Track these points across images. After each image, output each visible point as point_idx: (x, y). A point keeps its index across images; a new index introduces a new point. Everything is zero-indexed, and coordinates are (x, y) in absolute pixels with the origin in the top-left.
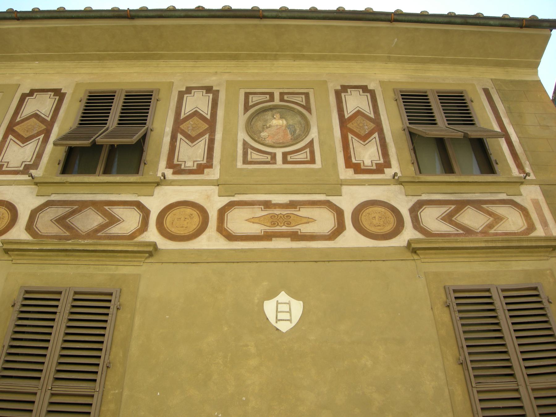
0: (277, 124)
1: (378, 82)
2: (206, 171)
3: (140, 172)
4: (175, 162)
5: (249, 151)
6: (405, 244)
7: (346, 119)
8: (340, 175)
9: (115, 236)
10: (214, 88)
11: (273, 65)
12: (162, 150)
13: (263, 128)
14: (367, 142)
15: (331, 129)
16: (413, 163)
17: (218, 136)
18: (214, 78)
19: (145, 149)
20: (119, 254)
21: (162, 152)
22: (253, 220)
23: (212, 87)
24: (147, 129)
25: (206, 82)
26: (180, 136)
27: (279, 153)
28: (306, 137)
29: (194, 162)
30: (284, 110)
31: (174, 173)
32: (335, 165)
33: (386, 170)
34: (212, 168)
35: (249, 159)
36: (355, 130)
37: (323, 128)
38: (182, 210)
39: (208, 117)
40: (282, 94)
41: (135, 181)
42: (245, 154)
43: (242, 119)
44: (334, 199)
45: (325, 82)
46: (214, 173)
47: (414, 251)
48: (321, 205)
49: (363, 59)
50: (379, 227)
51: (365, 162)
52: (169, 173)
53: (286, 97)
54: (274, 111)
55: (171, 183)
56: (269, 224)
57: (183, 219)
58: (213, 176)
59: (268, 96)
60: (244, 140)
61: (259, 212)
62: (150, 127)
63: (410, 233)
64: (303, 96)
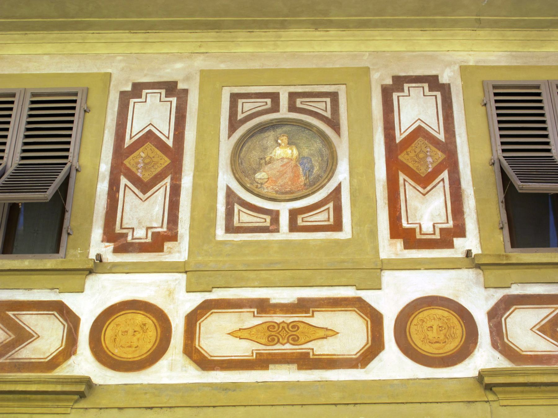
0: (283, 155)
1: (457, 67)
2: (167, 245)
3: (62, 250)
4: (118, 230)
5: (237, 207)
6: (476, 374)
7: (397, 145)
8: (381, 250)
9: (25, 363)
10: (180, 86)
11: (280, 37)
12: (96, 206)
13: (260, 164)
14: (429, 188)
15: (371, 164)
16: (502, 228)
17: (187, 182)
18: (179, 65)
19: (68, 207)
20: (34, 397)
21: (96, 212)
22: (239, 334)
23: (176, 83)
24: (70, 168)
25: (166, 74)
26: (124, 181)
27: (284, 232)
28: (329, 180)
29: (148, 228)
30: (295, 130)
31: (116, 251)
32: (373, 233)
33: (457, 241)
34: (177, 241)
35: (236, 223)
36: (411, 165)
37: (358, 165)
38: (130, 316)
39: (170, 143)
40: (293, 96)
41: (54, 267)
42: (229, 214)
43: (226, 146)
44: (368, 296)
45: (367, 70)
46: (178, 252)
47: (489, 388)
48: (347, 305)
49: (434, 25)
50: (437, 345)
51: (423, 227)
52: (107, 251)
53: (299, 103)
54: (279, 131)
55: (114, 268)
56: (264, 341)
57: (131, 332)
58: (177, 255)
59: (269, 101)
60: (228, 188)
61: (250, 320)
62: (75, 164)
63: (485, 357)
64: (328, 100)
